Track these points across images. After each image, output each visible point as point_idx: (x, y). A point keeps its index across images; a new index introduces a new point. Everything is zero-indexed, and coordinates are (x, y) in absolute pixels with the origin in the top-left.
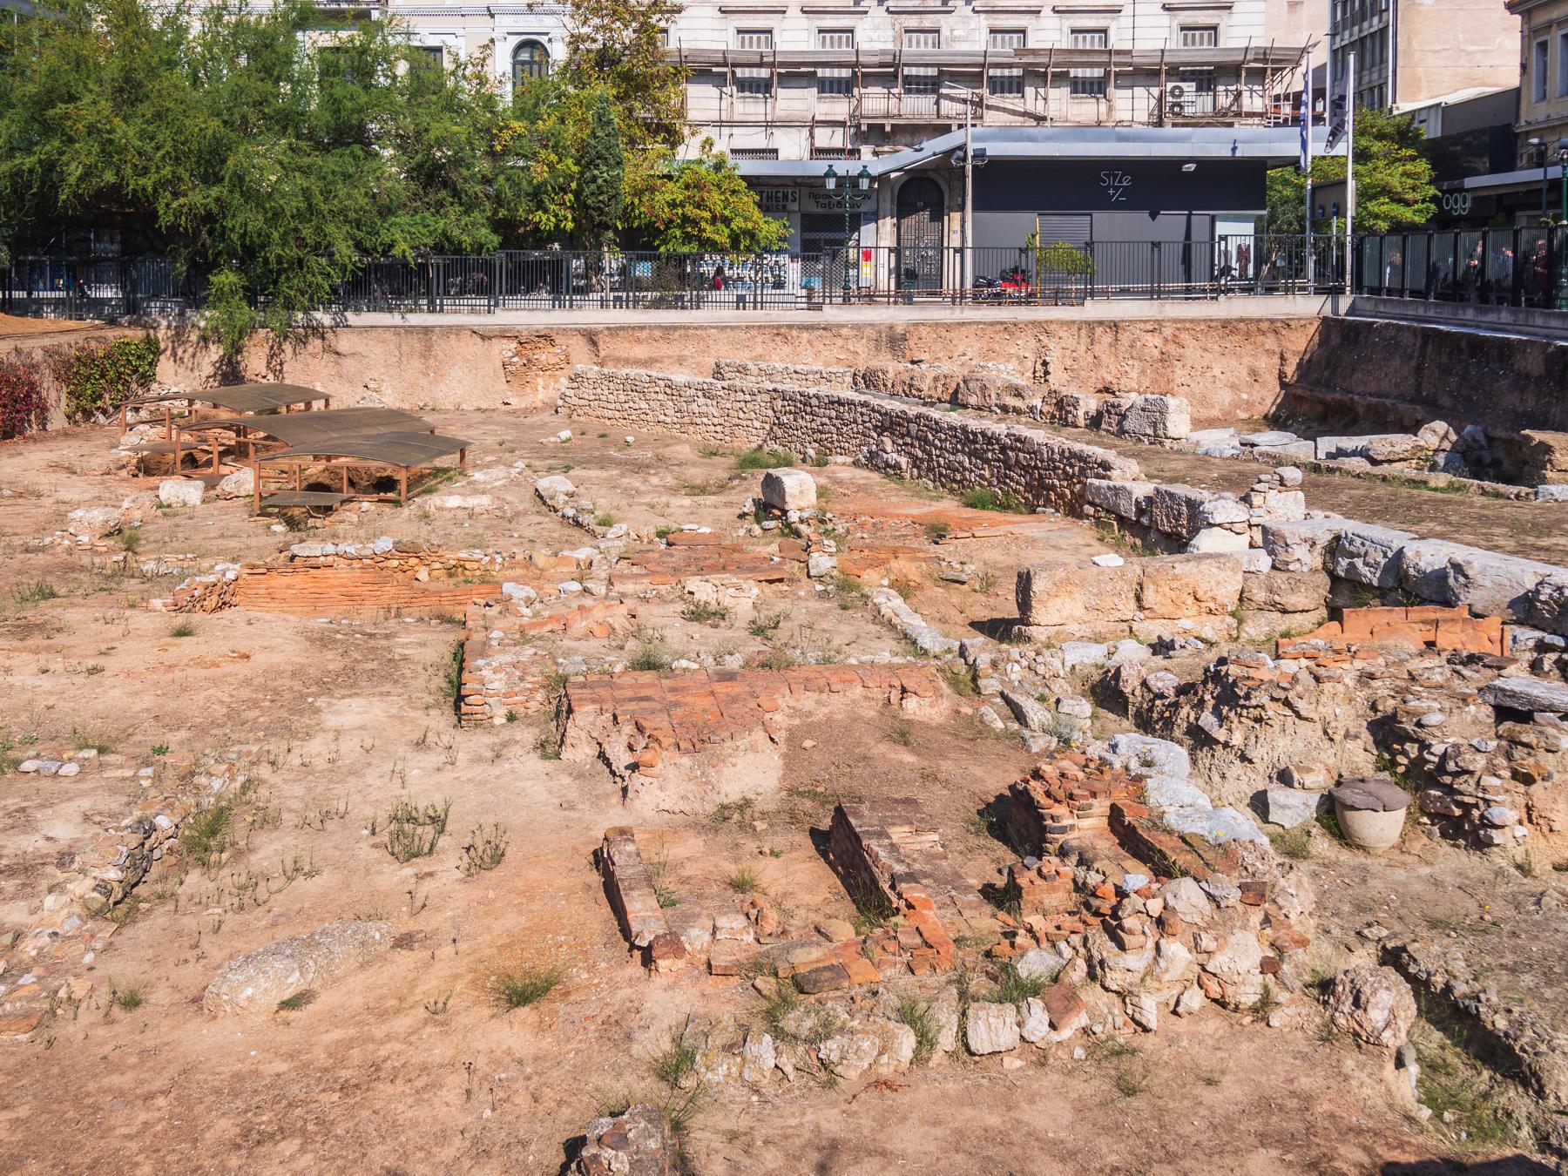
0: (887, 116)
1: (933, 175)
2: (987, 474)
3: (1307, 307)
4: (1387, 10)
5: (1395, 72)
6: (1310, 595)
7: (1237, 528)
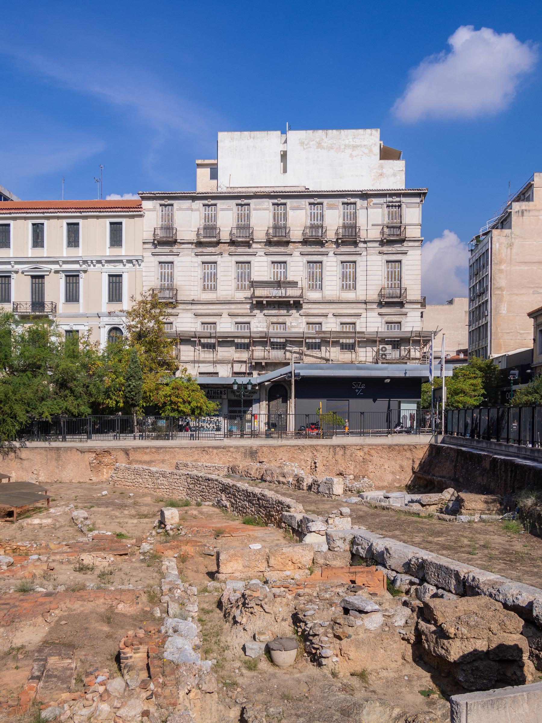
0: (264, 359)
1: (283, 384)
2: (253, 509)
3: (425, 439)
4: (488, 315)
5: (491, 341)
6: (341, 561)
7: (321, 533)
